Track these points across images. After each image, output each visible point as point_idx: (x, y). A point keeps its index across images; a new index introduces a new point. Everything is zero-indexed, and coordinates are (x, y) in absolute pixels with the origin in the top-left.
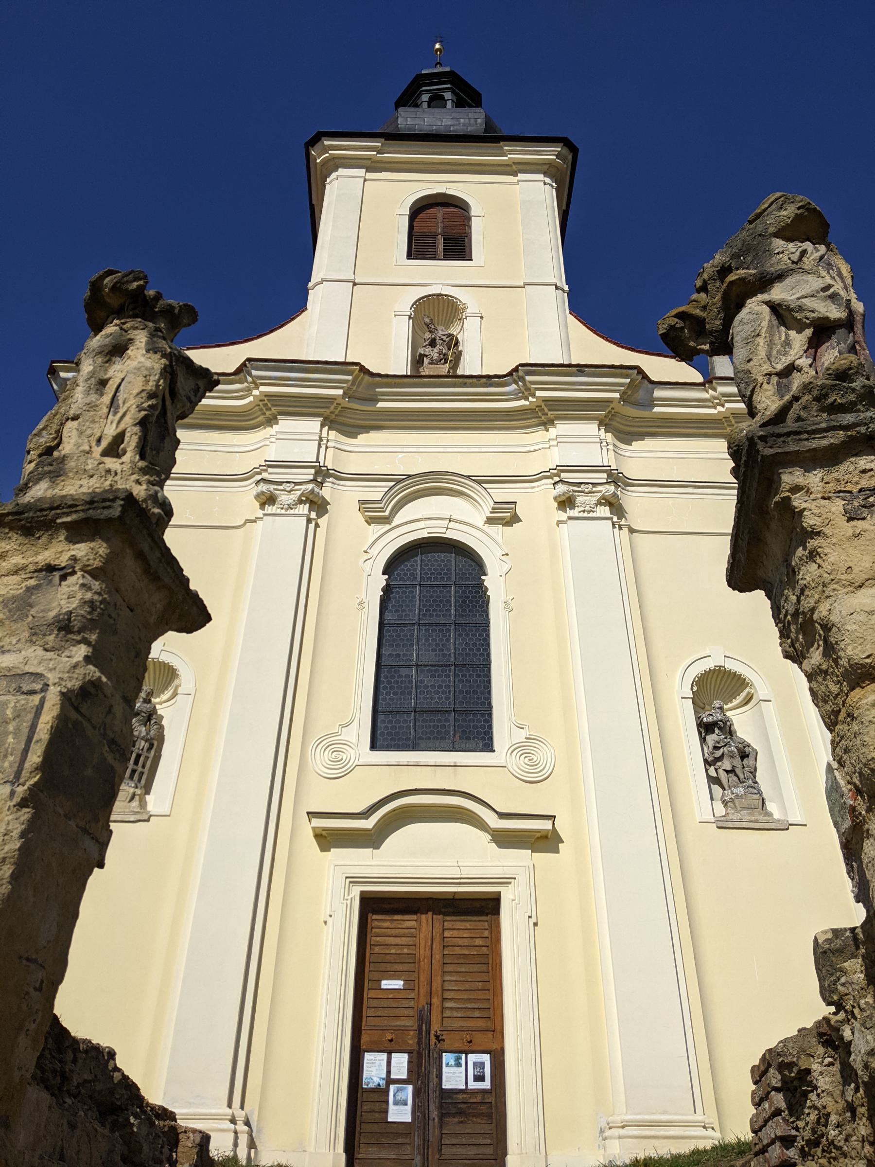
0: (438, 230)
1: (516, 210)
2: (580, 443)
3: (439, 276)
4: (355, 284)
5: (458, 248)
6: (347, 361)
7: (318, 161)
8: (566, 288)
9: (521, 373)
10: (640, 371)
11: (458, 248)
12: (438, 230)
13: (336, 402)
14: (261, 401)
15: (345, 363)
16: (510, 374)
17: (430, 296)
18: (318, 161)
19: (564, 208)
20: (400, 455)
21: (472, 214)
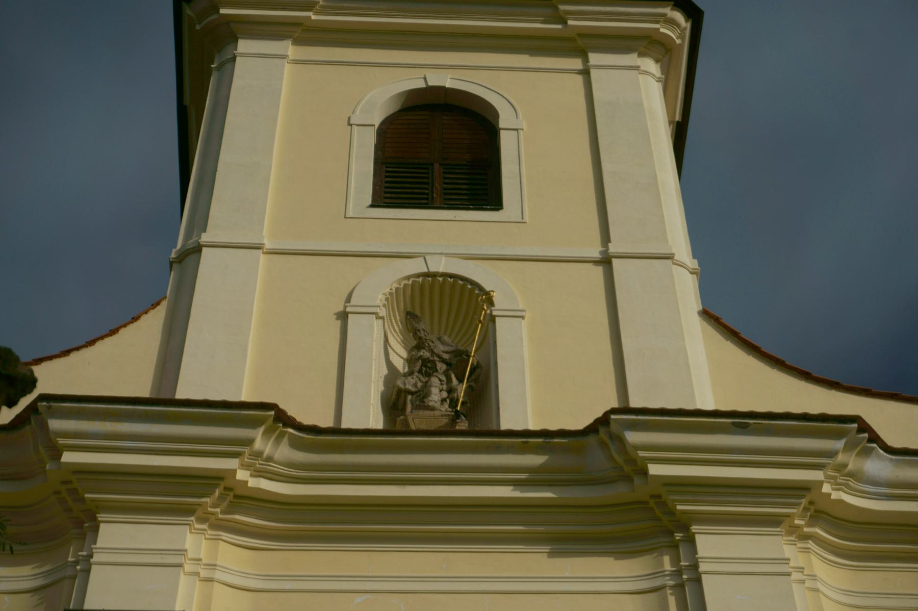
0: (440, 155)
3: (442, 238)
4: (606, 262)
5: (478, 185)
6: (344, 425)
7: (198, 27)
8: (693, 264)
9: (614, 427)
10: (864, 427)
11: (478, 185)
12: (440, 155)
13: (223, 484)
14: (65, 482)
15: (336, 431)
16: (592, 429)
17: (451, 276)
18: (198, 27)
19: (678, 118)
20: (359, 598)
21: (502, 124)
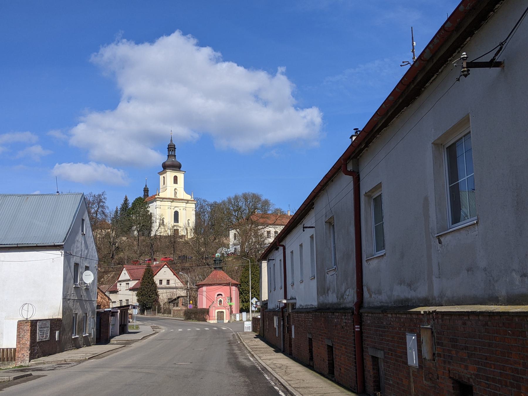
0: (176, 179)
1: (181, 176)
2: (184, 205)
3: (175, 186)
12: (176, 179)
